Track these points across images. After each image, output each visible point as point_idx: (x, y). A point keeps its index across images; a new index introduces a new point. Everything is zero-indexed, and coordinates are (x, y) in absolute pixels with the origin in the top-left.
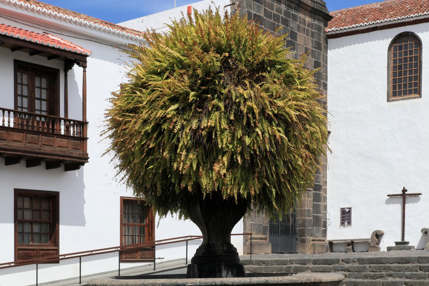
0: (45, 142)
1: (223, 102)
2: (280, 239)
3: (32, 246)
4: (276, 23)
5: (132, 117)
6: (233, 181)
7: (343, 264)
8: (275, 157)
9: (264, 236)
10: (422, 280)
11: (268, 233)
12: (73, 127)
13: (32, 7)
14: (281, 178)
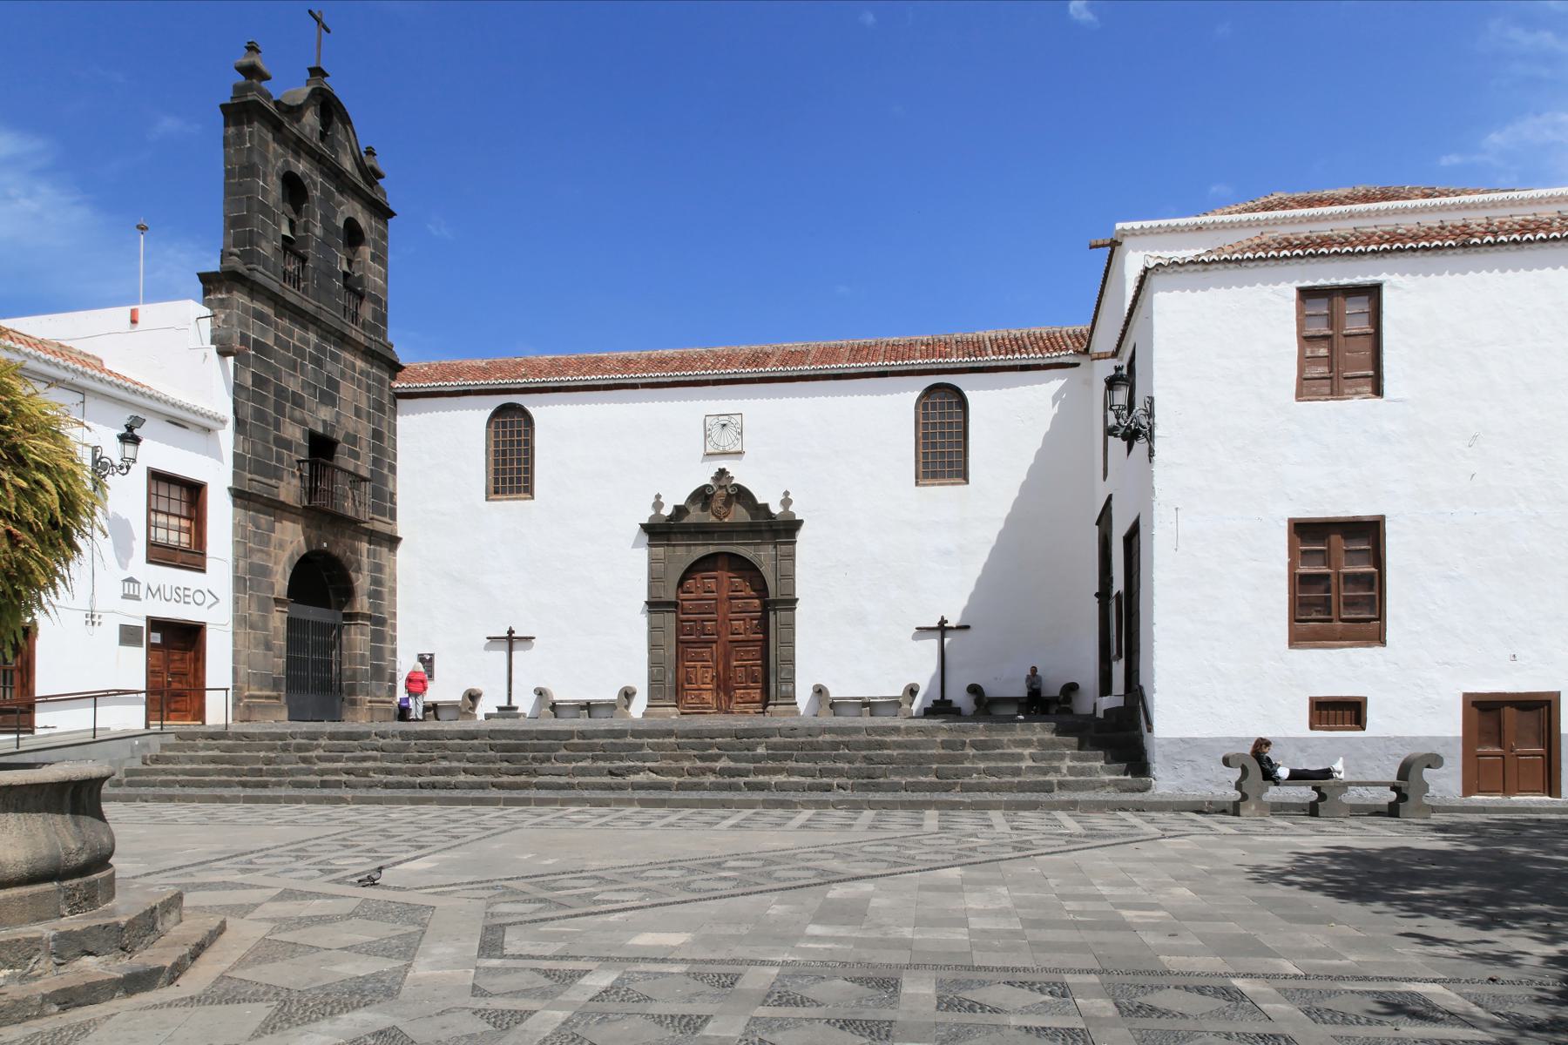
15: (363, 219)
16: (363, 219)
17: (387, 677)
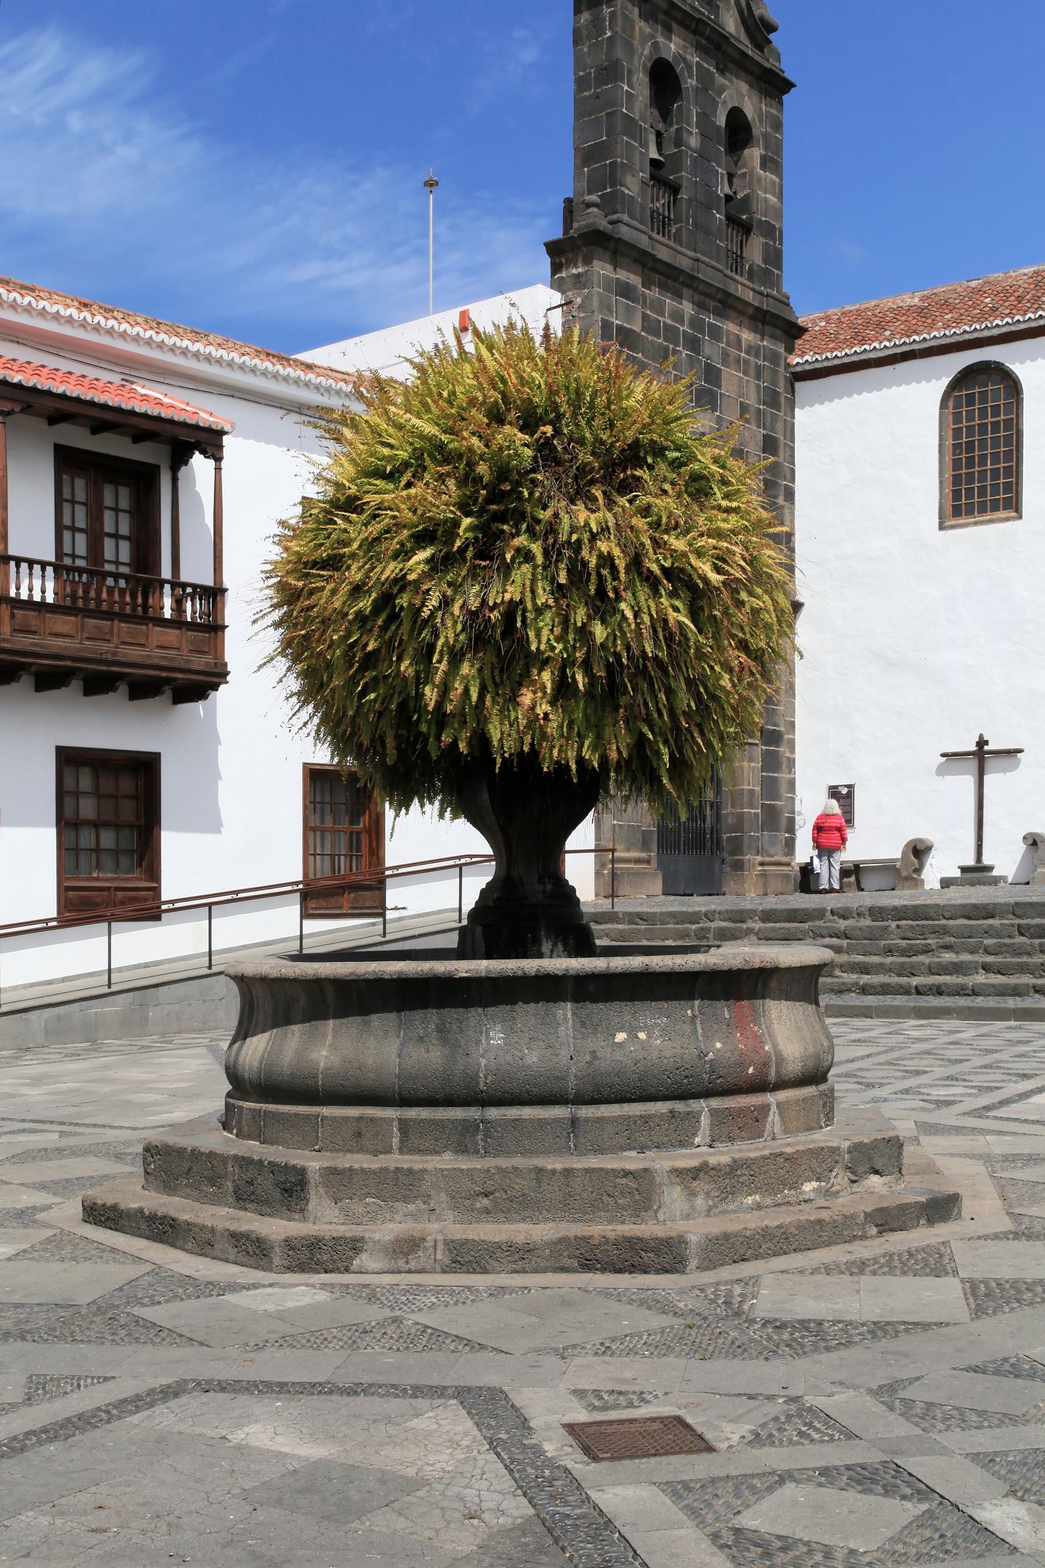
0: (123, 637)
1: (539, 543)
2: (683, 861)
3: (97, 879)
4: (671, 346)
5: (327, 580)
6: (565, 730)
7: (834, 921)
8: (665, 672)
9: (644, 855)
10: (1025, 959)
11: (655, 847)
12: (192, 601)
13: (96, 321)
14: (682, 719)
15: (751, 107)
16: (751, 107)
17: (783, 823)
